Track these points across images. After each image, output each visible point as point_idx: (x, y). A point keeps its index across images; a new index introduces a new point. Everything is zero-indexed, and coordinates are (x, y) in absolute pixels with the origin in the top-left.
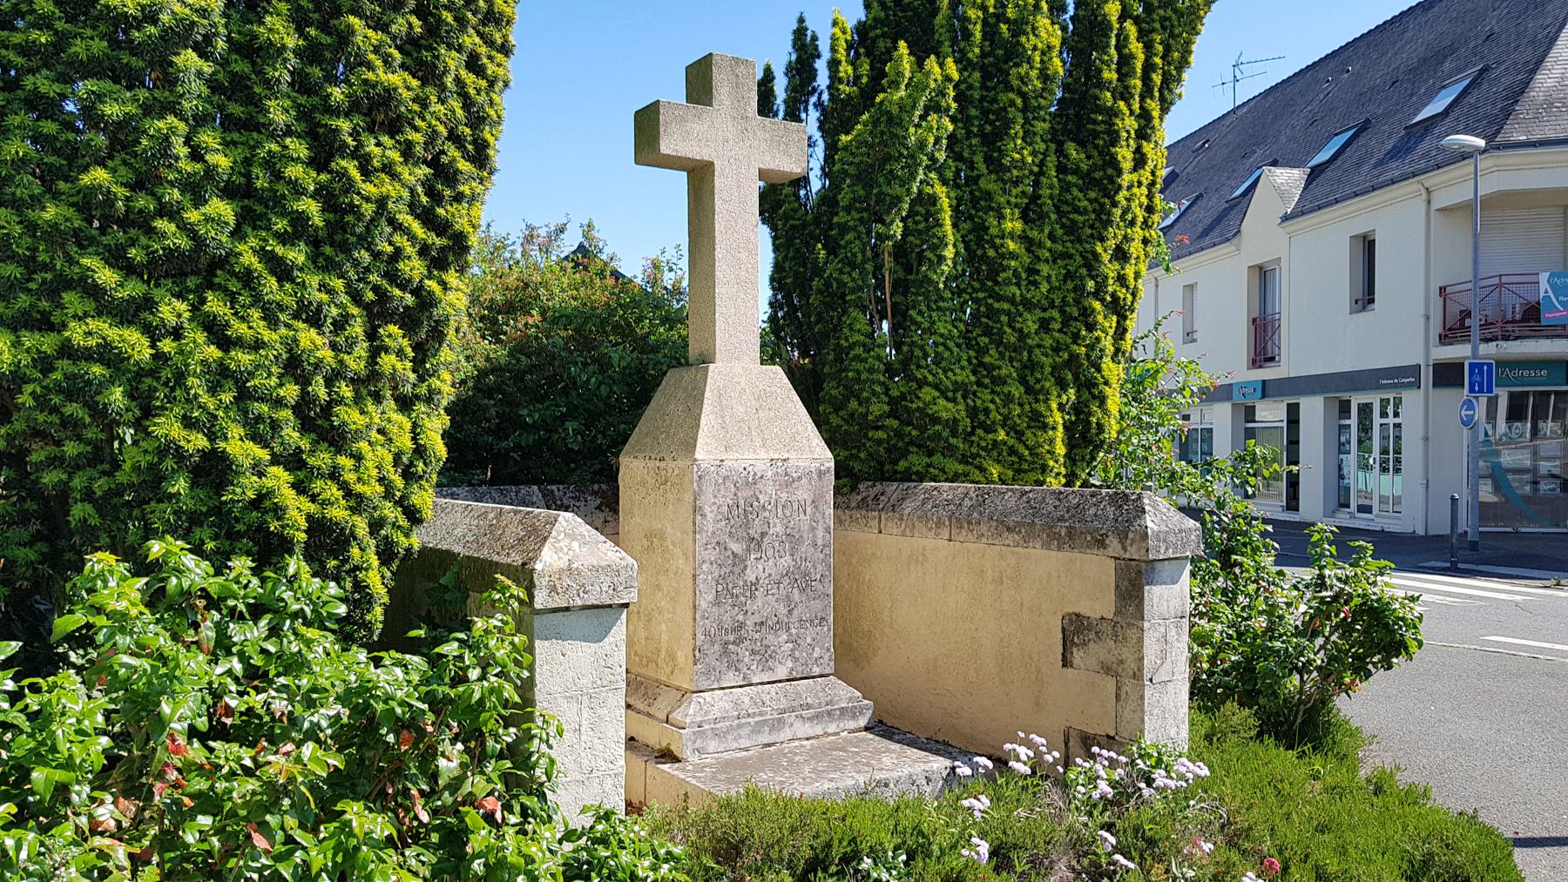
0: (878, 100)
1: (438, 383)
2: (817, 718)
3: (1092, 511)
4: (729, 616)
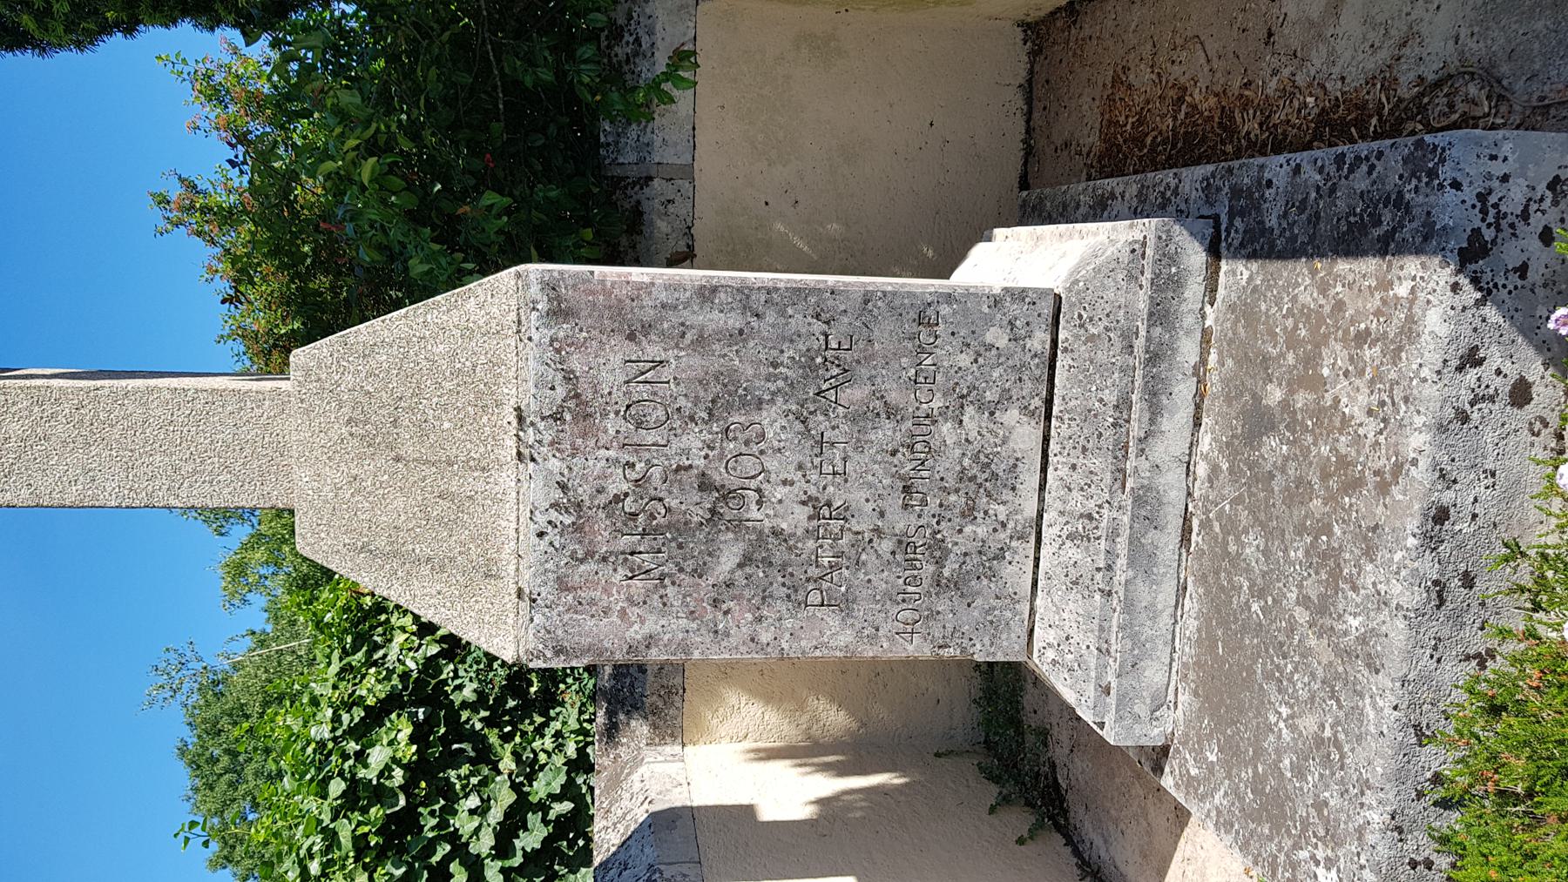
2: (1155, 396)
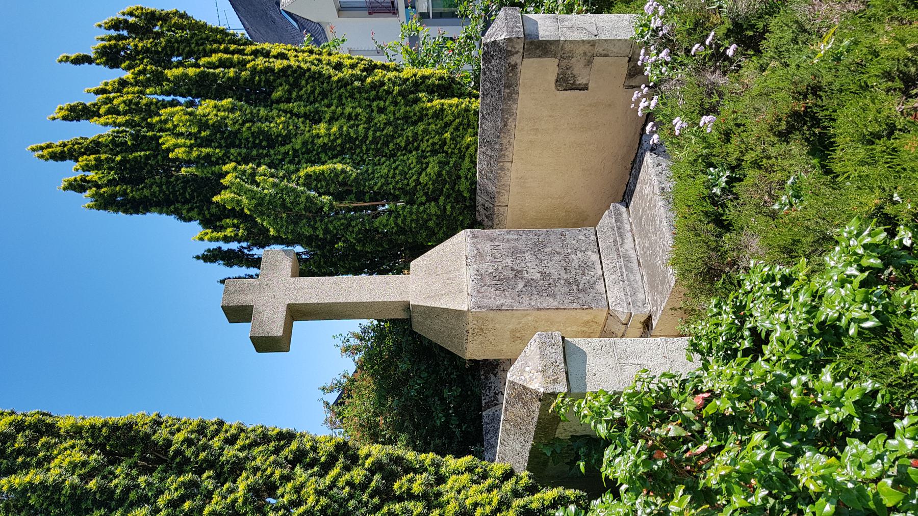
0: (248, 213)
1: (427, 460)
2: (621, 236)
3: (494, 73)
4: (561, 289)
